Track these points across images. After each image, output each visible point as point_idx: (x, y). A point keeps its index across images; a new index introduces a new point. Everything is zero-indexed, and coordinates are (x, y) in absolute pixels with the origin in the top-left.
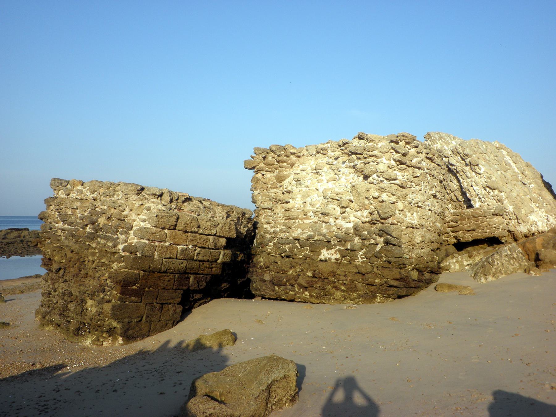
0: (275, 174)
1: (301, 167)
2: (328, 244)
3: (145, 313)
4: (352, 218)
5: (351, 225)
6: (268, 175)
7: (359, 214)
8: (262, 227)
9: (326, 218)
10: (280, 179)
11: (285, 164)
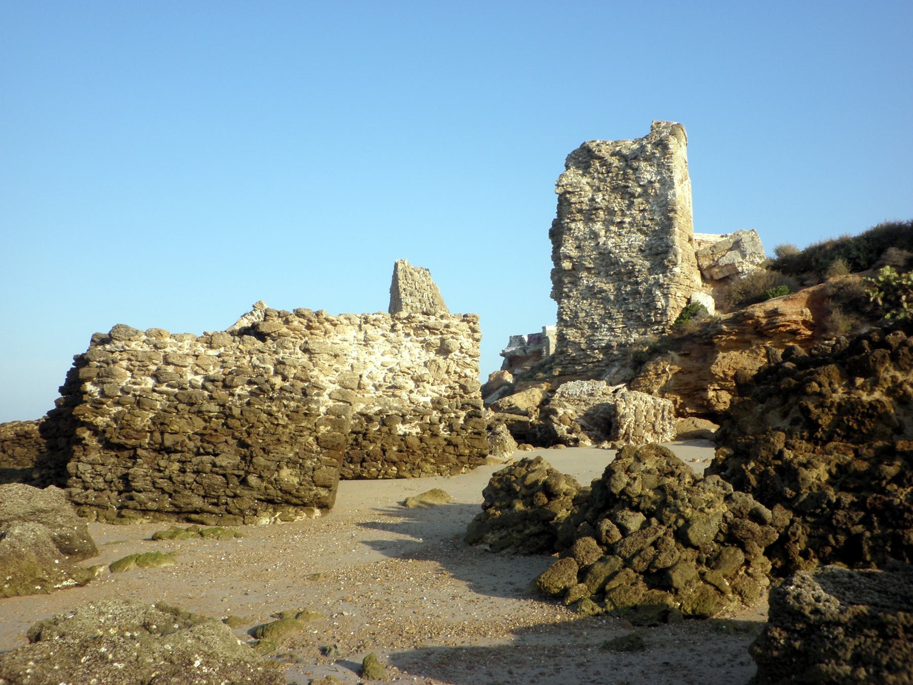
1: (340, 336)
5: (428, 399)
7: (435, 388)
9: (397, 392)
11: (318, 332)
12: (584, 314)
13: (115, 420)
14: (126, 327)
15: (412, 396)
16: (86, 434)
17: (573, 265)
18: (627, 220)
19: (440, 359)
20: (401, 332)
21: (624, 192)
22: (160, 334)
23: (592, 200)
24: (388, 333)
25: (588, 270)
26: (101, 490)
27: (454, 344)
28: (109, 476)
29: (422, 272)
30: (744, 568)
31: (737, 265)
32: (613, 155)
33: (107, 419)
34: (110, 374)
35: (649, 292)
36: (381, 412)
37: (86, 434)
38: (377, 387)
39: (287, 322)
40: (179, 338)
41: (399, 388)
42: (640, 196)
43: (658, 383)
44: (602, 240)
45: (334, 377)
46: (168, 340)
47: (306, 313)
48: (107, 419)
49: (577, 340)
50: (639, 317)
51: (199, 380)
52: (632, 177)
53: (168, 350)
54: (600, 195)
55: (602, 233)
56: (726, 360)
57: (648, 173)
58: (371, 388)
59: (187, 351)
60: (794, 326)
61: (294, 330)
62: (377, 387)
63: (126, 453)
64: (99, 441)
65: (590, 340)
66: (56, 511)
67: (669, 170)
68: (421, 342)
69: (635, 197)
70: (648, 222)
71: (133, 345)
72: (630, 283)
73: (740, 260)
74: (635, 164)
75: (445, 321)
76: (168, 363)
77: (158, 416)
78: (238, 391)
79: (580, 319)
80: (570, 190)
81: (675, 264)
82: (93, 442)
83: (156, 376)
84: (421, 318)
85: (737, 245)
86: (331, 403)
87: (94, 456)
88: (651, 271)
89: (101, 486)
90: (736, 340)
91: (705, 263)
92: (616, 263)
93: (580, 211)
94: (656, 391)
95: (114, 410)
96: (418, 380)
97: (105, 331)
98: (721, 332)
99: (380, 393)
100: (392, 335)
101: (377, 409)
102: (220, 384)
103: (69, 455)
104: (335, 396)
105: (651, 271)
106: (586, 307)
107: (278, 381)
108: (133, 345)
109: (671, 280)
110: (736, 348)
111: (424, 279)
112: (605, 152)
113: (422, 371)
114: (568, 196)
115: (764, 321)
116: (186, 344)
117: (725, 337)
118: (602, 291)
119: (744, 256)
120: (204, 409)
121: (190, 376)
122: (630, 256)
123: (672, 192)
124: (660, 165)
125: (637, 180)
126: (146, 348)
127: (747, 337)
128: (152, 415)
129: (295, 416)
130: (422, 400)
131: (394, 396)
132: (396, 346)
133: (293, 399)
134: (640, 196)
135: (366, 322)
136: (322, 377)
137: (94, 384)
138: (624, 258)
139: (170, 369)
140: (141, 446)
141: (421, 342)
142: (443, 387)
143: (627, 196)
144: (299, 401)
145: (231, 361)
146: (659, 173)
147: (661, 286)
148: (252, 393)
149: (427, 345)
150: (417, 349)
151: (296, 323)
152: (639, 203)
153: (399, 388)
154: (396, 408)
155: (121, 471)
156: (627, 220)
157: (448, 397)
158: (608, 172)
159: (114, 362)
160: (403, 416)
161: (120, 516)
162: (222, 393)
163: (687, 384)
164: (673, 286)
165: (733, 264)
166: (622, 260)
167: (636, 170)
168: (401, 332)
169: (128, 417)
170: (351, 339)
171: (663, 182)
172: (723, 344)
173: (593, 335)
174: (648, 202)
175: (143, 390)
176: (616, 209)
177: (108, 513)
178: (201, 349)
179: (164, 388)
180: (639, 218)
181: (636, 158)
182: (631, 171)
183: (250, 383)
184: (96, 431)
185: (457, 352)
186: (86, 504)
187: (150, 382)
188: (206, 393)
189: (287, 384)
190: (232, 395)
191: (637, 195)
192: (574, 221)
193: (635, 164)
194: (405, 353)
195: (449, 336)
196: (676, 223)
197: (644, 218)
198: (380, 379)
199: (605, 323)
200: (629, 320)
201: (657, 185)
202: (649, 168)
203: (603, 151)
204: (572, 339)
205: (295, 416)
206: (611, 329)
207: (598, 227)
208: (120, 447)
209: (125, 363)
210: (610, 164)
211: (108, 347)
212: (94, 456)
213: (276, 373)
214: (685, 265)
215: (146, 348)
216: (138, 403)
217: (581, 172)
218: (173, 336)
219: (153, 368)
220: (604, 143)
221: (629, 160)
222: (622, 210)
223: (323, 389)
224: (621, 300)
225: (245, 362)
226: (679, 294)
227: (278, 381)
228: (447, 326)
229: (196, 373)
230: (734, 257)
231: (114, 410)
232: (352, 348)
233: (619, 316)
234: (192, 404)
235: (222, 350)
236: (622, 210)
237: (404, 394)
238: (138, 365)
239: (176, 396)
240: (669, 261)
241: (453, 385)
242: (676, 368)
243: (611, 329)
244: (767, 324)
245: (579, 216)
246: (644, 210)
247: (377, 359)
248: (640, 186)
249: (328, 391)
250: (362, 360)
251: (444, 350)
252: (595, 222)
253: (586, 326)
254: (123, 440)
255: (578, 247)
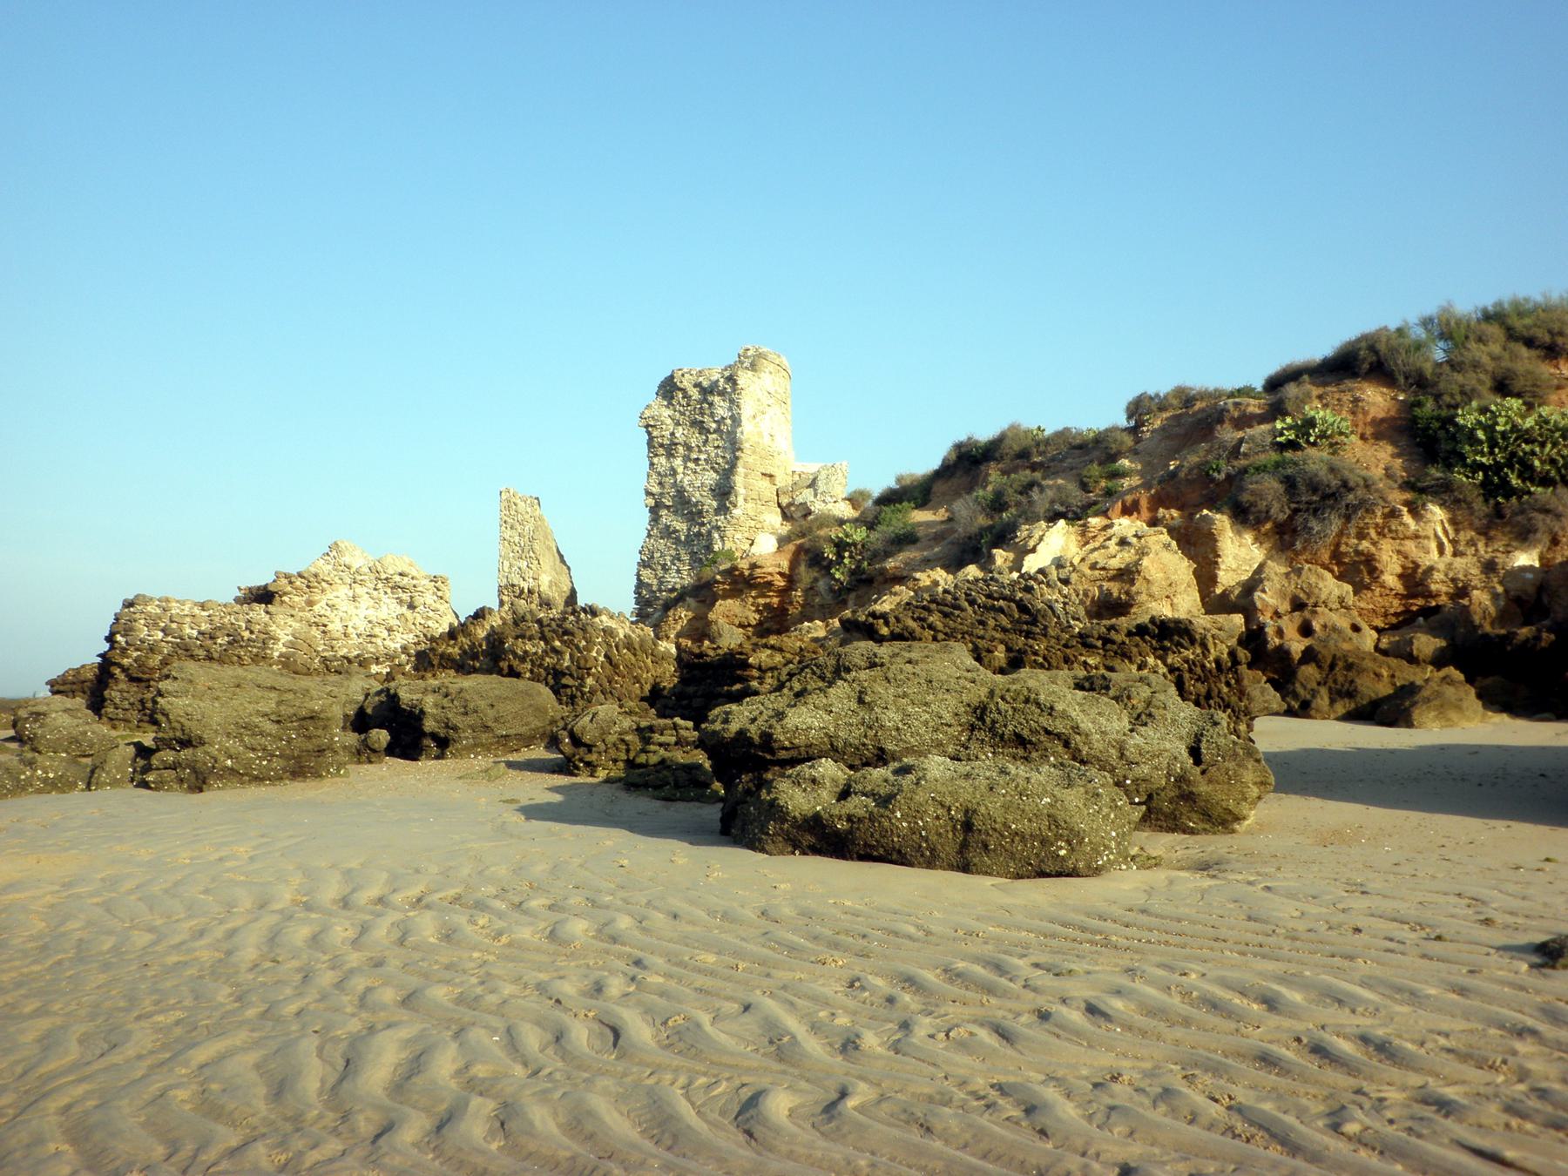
0: (304, 598)
1: (335, 594)
2: (377, 661)
3: (870, 1122)
4: (399, 639)
5: (398, 646)
6: (296, 599)
7: (405, 636)
8: (1294, 684)
9: (374, 640)
10: (310, 603)
11: (316, 590)
12: (659, 555)
13: (135, 661)
14: (144, 596)
15: (385, 642)
16: (117, 671)
17: (656, 502)
18: (703, 457)
19: (408, 613)
20: (381, 591)
21: (699, 426)
22: (167, 600)
23: (672, 434)
24: (371, 591)
25: (668, 507)
26: (127, 710)
27: (418, 601)
28: (132, 700)
29: (528, 502)
30: (671, 780)
31: (809, 504)
32: (696, 386)
33: (130, 660)
34: (131, 629)
35: (709, 533)
36: (358, 656)
37: (117, 671)
38: (359, 635)
39: (291, 583)
40: (183, 603)
41: (375, 636)
42: (715, 432)
43: (674, 628)
44: (679, 477)
45: (289, 631)
46: (174, 604)
47: (306, 575)
48: (130, 660)
49: (650, 582)
50: (701, 559)
51: (195, 633)
52: (707, 412)
53: (173, 612)
54: (680, 428)
55: (680, 470)
56: (721, 608)
57: (721, 408)
58: (354, 636)
59: (186, 613)
60: (770, 578)
61: (296, 589)
62: (359, 635)
63: (143, 684)
64: (126, 676)
65: (661, 583)
66: (77, 710)
67: (738, 406)
68: (397, 599)
69: (710, 433)
70: (720, 460)
71: (149, 608)
72: (698, 524)
73: (812, 499)
74: (710, 398)
75: (414, 582)
76: (172, 622)
77: (164, 658)
78: (219, 641)
79: (655, 560)
80: (652, 423)
81: (735, 506)
82: (122, 677)
83: (163, 630)
84: (397, 578)
85: (813, 484)
86: (284, 650)
87: (123, 686)
88: (717, 512)
89: (127, 707)
90: (730, 590)
91: (785, 501)
92: (689, 502)
93: (662, 445)
94: (672, 636)
95: (135, 654)
96: (390, 630)
97: (131, 597)
98: (718, 582)
99: (361, 640)
100: (375, 593)
101: (356, 653)
102: (207, 636)
103: (106, 686)
104: (288, 644)
105: (717, 512)
106: (662, 547)
107: (246, 634)
108: (149, 608)
109: (729, 522)
110: (731, 597)
111: (529, 510)
112: (686, 383)
113: (393, 622)
114: (650, 429)
115: (747, 573)
116: (187, 608)
117: (721, 587)
118: (676, 531)
119: (816, 495)
120: (194, 653)
121: (188, 630)
122: (701, 495)
123: (740, 429)
124: (732, 401)
125: (712, 415)
126: (158, 611)
127: (740, 586)
128: (160, 658)
129: (256, 658)
130: (392, 646)
131: (371, 642)
132: (378, 601)
133: (255, 647)
134: (715, 432)
135: (355, 582)
136: (278, 631)
137: (122, 636)
138: (696, 497)
139: (174, 626)
140: (153, 680)
141: (397, 599)
142: (411, 636)
143: (704, 432)
144: (259, 648)
145: (217, 619)
146: (730, 409)
147: (718, 528)
148: (229, 643)
149: (401, 602)
150: (393, 604)
151: (298, 583)
152: (714, 440)
153: (375, 636)
154: (371, 653)
155: (140, 696)
156: (703, 457)
157: (415, 644)
158: (688, 405)
159: (135, 621)
160: (377, 659)
161: (138, 727)
162: (209, 642)
163: (697, 629)
164: (729, 528)
165: (806, 503)
166: (694, 500)
167: (711, 404)
168: (381, 591)
169: (143, 659)
170: (344, 597)
171: (732, 418)
172: (720, 593)
173: (663, 577)
174: (722, 438)
175: (155, 641)
176: (693, 445)
177: (131, 725)
178: (197, 611)
179: (169, 639)
180: (713, 455)
181: (711, 392)
182: (706, 406)
183: (228, 635)
184: (124, 670)
185: (422, 607)
186: (117, 719)
187: (160, 635)
188: (198, 642)
189: (254, 636)
190: (215, 644)
191: (712, 430)
192: (656, 455)
193: (710, 398)
194: (384, 607)
195: (416, 594)
196: (740, 463)
197: (717, 456)
198: (361, 630)
199: (674, 565)
200: (695, 562)
201: (729, 422)
202: (722, 403)
203: (685, 383)
204: (647, 580)
205: (256, 658)
206: (678, 571)
207: (678, 462)
208: (139, 680)
209: (142, 622)
210: (691, 397)
211: (132, 609)
212: (123, 686)
213: (247, 628)
214: (750, 505)
215: (158, 611)
216: (151, 649)
217: (666, 403)
218: (178, 602)
219: (163, 625)
220: (689, 373)
221: (707, 391)
222: (698, 446)
223: (279, 640)
224: (688, 542)
225: (226, 620)
226: (738, 536)
227: (246, 634)
228: (415, 586)
229: (192, 629)
230: (806, 496)
231: (135, 654)
232: (343, 603)
233: (686, 558)
234: (187, 650)
235: (211, 612)
236: (698, 446)
237: (379, 641)
238: (153, 622)
239: (177, 644)
240: (730, 503)
241: (419, 633)
242: (690, 614)
243: (678, 571)
244: (750, 575)
245: (661, 451)
246: (718, 447)
247: (362, 612)
248: (715, 421)
249: (282, 641)
250: (349, 613)
251: (412, 607)
252: (674, 457)
253: (660, 567)
254: (141, 675)
255: (660, 483)
